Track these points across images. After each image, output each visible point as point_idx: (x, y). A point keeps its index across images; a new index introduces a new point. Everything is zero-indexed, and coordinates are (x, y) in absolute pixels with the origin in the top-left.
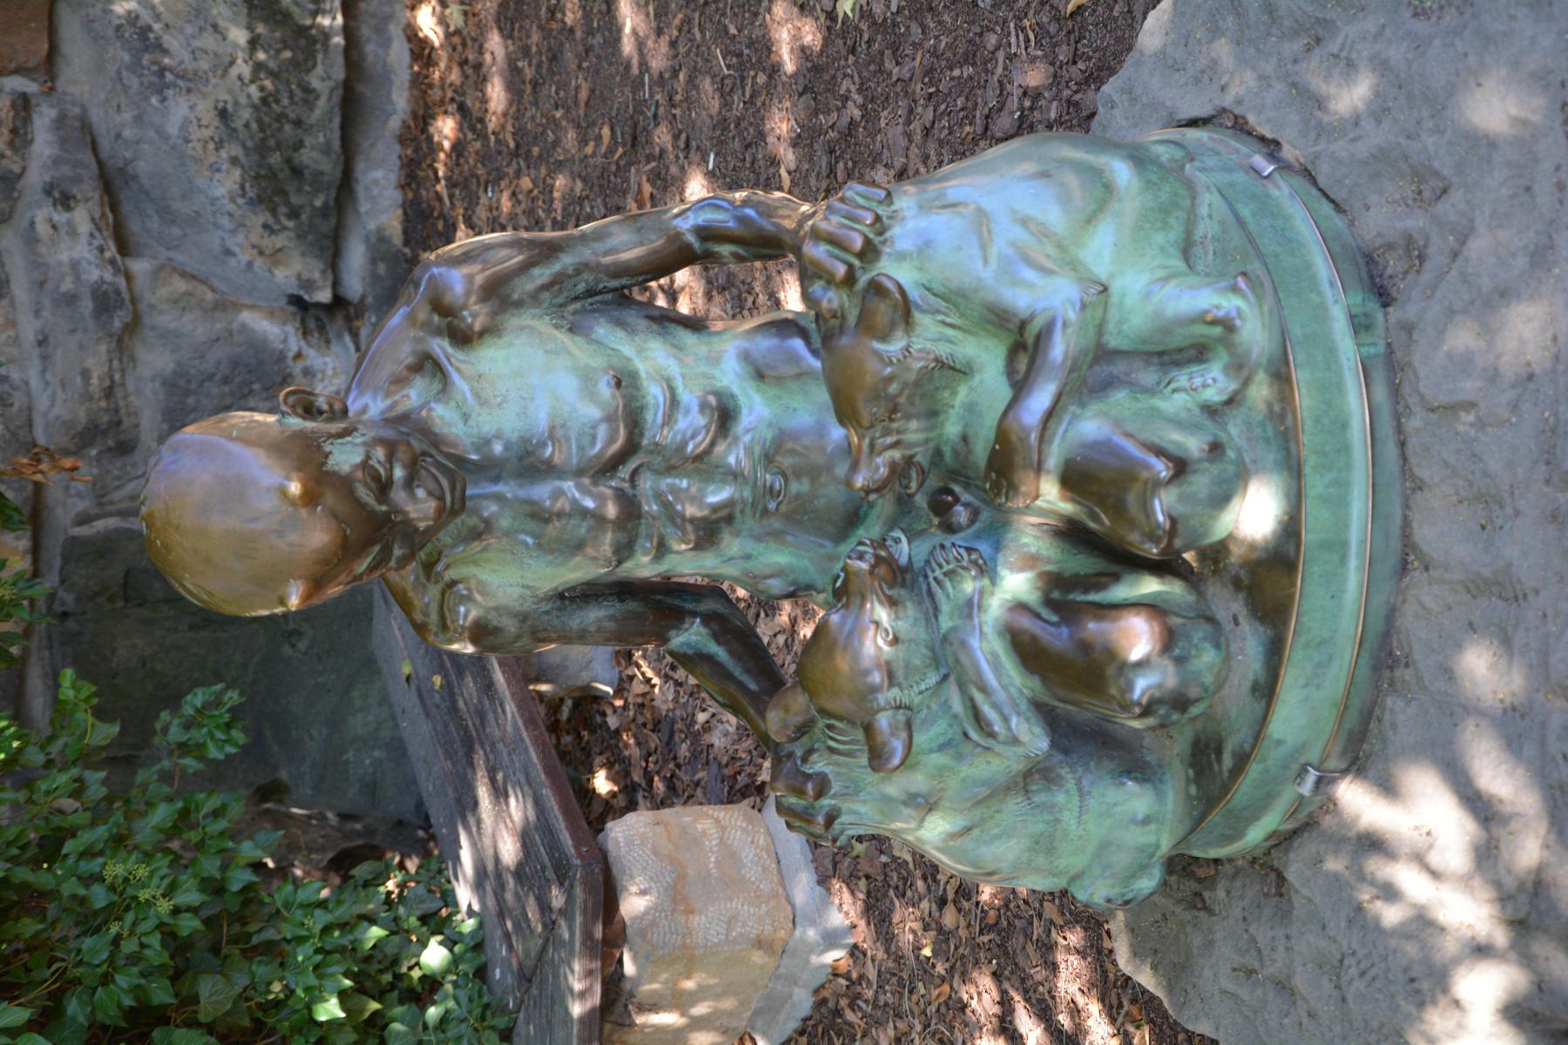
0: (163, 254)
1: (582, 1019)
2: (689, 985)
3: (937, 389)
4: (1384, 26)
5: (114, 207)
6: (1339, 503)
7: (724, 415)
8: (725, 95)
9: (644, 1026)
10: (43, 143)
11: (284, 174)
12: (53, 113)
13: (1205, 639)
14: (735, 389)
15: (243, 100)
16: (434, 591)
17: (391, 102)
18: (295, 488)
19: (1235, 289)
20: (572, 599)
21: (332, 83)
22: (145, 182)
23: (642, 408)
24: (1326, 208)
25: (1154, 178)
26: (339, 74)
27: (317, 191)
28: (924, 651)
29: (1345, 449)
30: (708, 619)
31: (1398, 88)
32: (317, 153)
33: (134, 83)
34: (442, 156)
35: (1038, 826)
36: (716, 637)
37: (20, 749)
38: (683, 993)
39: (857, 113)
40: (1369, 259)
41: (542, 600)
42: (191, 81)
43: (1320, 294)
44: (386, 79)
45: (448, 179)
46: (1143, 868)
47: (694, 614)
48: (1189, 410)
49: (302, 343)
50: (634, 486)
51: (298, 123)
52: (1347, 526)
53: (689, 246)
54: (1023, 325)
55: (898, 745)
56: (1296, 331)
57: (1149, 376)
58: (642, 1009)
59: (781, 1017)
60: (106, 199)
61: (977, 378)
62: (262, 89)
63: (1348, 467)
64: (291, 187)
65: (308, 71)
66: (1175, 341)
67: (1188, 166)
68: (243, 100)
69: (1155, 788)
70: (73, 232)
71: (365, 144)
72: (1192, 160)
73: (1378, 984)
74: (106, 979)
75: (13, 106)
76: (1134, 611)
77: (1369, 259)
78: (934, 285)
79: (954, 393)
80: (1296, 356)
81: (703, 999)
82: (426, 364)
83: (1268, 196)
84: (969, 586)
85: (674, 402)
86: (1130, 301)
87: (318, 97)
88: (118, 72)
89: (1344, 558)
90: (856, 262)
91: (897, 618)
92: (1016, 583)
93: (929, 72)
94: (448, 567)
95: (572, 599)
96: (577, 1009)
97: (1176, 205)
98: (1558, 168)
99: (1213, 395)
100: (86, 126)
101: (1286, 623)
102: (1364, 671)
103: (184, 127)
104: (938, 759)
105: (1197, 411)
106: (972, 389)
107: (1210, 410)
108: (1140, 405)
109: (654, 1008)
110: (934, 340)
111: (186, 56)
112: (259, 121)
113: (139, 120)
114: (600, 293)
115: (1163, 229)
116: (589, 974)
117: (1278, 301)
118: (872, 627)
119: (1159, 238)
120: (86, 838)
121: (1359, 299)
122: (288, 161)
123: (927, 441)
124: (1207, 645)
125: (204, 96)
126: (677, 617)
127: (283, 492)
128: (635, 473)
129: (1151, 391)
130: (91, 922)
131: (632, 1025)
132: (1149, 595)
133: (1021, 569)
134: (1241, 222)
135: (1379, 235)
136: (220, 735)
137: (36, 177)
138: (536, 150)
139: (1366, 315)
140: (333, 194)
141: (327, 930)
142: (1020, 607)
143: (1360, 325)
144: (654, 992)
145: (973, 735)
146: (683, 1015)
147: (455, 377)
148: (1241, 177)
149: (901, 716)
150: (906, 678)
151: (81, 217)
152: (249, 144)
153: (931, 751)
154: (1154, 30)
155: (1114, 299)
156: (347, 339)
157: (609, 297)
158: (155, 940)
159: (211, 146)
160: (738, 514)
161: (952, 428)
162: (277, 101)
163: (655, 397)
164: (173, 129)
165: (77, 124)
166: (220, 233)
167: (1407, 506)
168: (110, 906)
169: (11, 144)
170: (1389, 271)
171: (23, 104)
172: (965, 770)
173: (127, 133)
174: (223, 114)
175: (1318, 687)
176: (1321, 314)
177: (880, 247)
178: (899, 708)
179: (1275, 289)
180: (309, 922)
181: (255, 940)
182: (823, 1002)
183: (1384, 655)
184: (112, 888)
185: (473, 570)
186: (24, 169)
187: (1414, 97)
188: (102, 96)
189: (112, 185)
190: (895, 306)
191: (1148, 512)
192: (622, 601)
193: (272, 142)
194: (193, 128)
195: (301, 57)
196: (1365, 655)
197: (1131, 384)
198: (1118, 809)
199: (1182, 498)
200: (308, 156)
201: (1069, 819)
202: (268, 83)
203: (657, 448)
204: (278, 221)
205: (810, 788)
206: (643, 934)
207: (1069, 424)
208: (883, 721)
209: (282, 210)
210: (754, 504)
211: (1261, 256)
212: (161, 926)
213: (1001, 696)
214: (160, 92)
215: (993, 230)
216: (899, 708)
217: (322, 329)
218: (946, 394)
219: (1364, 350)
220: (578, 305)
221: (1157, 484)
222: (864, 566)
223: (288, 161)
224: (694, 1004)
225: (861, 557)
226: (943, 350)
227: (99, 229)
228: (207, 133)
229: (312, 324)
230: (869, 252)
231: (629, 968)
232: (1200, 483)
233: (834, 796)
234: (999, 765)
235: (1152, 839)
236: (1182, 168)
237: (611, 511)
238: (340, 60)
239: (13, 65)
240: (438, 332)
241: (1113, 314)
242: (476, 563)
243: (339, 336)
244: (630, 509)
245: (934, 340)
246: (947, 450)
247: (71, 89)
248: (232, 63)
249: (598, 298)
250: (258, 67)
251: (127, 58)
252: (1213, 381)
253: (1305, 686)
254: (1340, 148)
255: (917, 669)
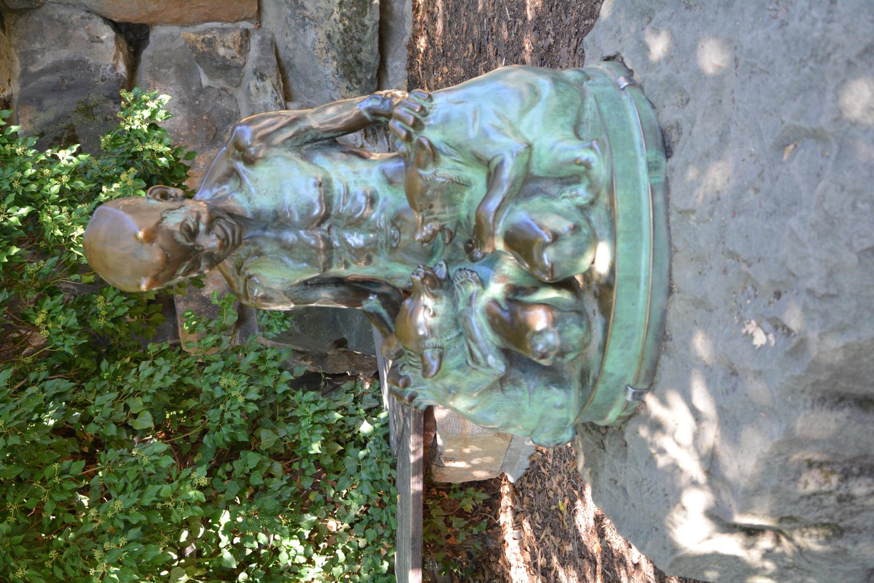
0: (306, 100)
1: (414, 464)
2: (467, 451)
3: (452, 193)
4: (673, 14)
5: (285, 80)
6: (634, 256)
7: (372, 200)
8: (509, 29)
9: (449, 468)
10: (254, 51)
11: (354, 64)
12: (259, 38)
13: (573, 322)
14: (378, 189)
15: (336, 30)
16: (242, 281)
17: (405, 29)
18: (141, 235)
19: (591, 147)
20: (311, 285)
21: (373, 22)
22: (298, 67)
23: (332, 197)
24: (647, 106)
25: (562, 89)
26: (377, 18)
27: (368, 72)
28: (449, 320)
29: (640, 230)
30: (381, 296)
31: (676, 43)
32: (369, 53)
33: (293, 23)
34: (421, 56)
35: (509, 406)
36: (384, 305)
37: (195, 325)
38: (465, 454)
39: (552, 41)
40: (664, 134)
41: (293, 286)
42: (316, 22)
43: (635, 151)
44: (403, 19)
45: (422, 66)
46: (563, 429)
47: (374, 293)
48: (569, 208)
49: (364, 141)
50: (329, 234)
51: (359, 40)
52: (640, 269)
53: (365, 118)
54: (488, 163)
55: (435, 364)
56: (619, 169)
57: (554, 190)
58: (447, 460)
59: (516, 467)
60: (280, 76)
61: (474, 188)
62: (344, 25)
63: (641, 239)
64: (357, 70)
65: (364, 16)
66: (564, 173)
67: (585, 83)
68: (336, 30)
69: (565, 391)
70: (265, 91)
71: (392, 49)
72: (588, 79)
73: (654, 495)
74: (218, 429)
75: (241, 35)
76: (538, 306)
77: (664, 134)
78: (449, 142)
79: (463, 195)
80: (618, 183)
81: (476, 457)
82: (233, 174)
83: (620, 99)
84: (473, 288)
85: (348, 193)
86: (543, 152)
87: (368, 28)
88: (286, 18)
89: (638, 285)
90: (412, 130)
91: (436, 304)
92: (496, 290)
93: (577, 21)
94: (246, 269)
95: (311, 285)
96: (412, 459)
97: (572, 103)
98: (733, 92)
99: (580, 200)
100: (273, 43)
101: (609, 316)
102: (650, 341)
103: (313, 43)
104: (455, 372)
105: (574, 208)
106: (471, 193)
107: (582, 209)
108: (544, 205)
109: (452, 459)
110: (449, 169)
111: (314, 11)
112: (343, 40)
113: (295, 40)
114: (320, 140)
115: (563, 115)
116: (418, 444)
117: (611, 154)
118: (423, 308)
119: (561, 120)
120: (214, 366)
121: (654, 154)
122: (355, 58)
123: (451, 218)
124: (574, 325)
125: (321, 28)
126: (366, 294)
127: (136, 236)
128: (329, 228)
129: (553, 197)
130: (216, 403)
131: (444, 467)
132: (547, 299)
133: (499, 282)
134: (600, 113)
135: (668, 121)
136: (279, 323)
137: (250, 66)
138: (449, 54)
139: (656, 162)
140: (376, 73)
141: (315, 413)
142: (495, 301)
143: (652, 167)
144: (450, 453)
145: (470, 362)
146: (468, 463)
147: (247, 181)
148: (610, 89)
149: (437, 352)
150: (440, 333)
151: (268, 84)
152: (339, 50)
153: (454, 368)
154: (605, 11)
155: (535, 151)
156: (385, 139)
157: (326, 141)
158: (238, 414)
159: (324, 51)
160: (380, 248)
161: (464, 213)
162: (351, 30)
163: (339, 191)
164: (309, 44)
165: (269, 42)
166: (329, 91)
167: (671, 261)
168: (223, 397)
169: (240, 52)
170: (673, 140)
171: (247, 33)
172: (469, 379)
173: (290, 46)
174: (329, 37)
175: (629, 348)
176: (634, 161)
177: (426, 123)
178: (435, 347)
179: (611, 148)
180: (307, 409)
181: (290, 415)
182: (533, 462)
183: (660, 335)
184: (224, 389)
185: (258, 271)
186: (245, 63)
187: (683, 52)
188: (280, 29)
189: (282, 69)
190: (428, 154)
191: (541, 259)
192: (337, 286)
193: (348, 49)
194: (317, 43)
195: (361, 10)
196: (650, 336)
197: (546, 193)
198: (547, 401)
199: (558, 253)
200: (364, 56)
201: (524, 403)
202: (347, 22)
203: (339, 216)
204: (352, 86)
205: (401, 382)
206: (443, 427)
207: (509, 212)
208: (428, 353)
209: (354, 80)
210: (386, 244)
211: (606, 131)
212: (240, 408)
213: (482, 345)
214: (303, 27)
215: (500, 114)
216: (435, 347)
217: (374, 134)
218: (458, 195)
219: (653, 180)
220: (309, 146)
221: (545, 245)
222: (418, 278)
223: (355, 58)
224: (472, 459)
225: (417, 275)
226: (453, 174)
227: (276, 90)
228: (322, 45)
229: (370, 132)
230: (418, 125)
231: (440, 442)
232: (567, 247)
233: (413, 387)
234: (482, 377)
235: (565, 416)
236: (582, 84)
237: (322, 245)
238: (377, 11)
239: (243, 17)
240: (238, 159)
241: (535, 158)
242: (260, 267)
243: (382, 138)
244: (329, 246)
245: (449, 169)
246: (463, 222)
247: (268, 26)
248: (332, 13)
249: (320, 142)
250: (343, 15)
251: (290, 12)
252: (581, 193)
253: (621, 348)
254: (652, 75)
255: (445, 329)
